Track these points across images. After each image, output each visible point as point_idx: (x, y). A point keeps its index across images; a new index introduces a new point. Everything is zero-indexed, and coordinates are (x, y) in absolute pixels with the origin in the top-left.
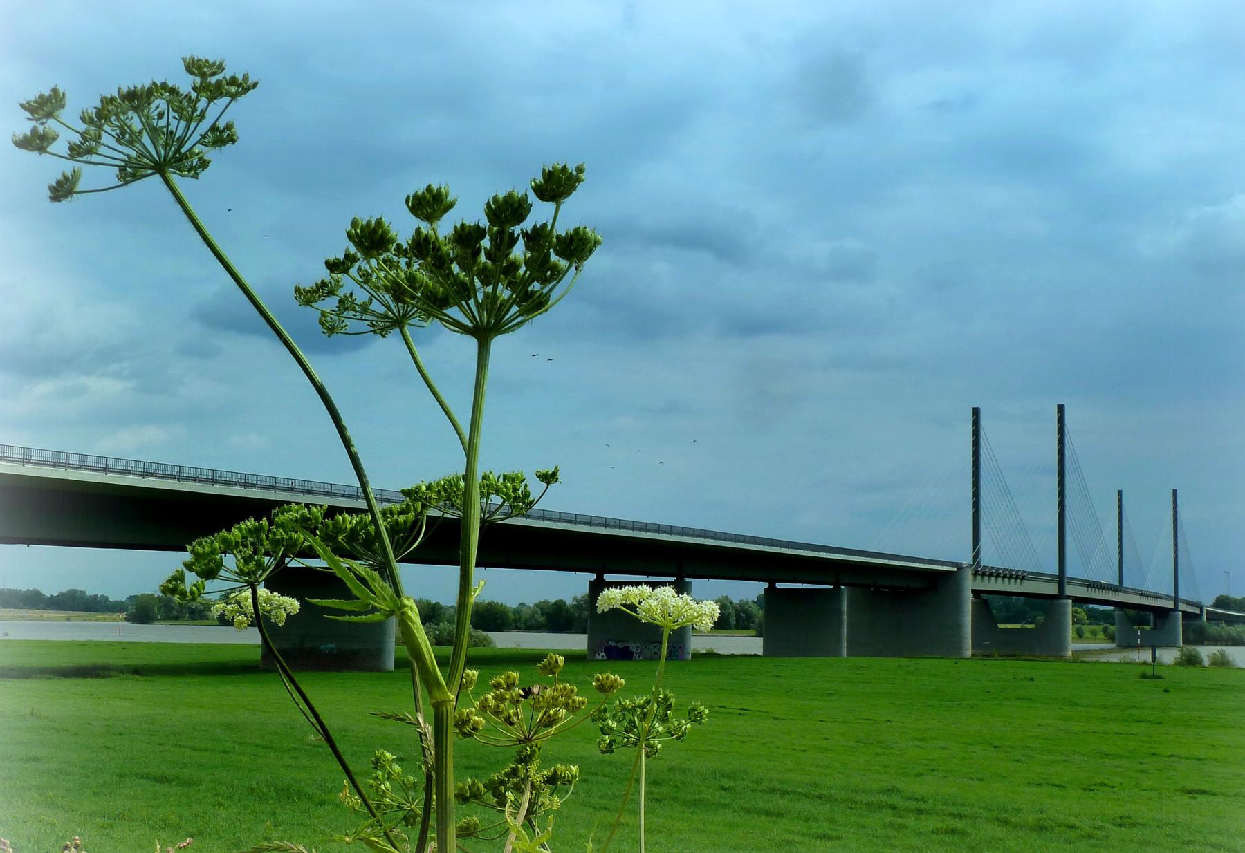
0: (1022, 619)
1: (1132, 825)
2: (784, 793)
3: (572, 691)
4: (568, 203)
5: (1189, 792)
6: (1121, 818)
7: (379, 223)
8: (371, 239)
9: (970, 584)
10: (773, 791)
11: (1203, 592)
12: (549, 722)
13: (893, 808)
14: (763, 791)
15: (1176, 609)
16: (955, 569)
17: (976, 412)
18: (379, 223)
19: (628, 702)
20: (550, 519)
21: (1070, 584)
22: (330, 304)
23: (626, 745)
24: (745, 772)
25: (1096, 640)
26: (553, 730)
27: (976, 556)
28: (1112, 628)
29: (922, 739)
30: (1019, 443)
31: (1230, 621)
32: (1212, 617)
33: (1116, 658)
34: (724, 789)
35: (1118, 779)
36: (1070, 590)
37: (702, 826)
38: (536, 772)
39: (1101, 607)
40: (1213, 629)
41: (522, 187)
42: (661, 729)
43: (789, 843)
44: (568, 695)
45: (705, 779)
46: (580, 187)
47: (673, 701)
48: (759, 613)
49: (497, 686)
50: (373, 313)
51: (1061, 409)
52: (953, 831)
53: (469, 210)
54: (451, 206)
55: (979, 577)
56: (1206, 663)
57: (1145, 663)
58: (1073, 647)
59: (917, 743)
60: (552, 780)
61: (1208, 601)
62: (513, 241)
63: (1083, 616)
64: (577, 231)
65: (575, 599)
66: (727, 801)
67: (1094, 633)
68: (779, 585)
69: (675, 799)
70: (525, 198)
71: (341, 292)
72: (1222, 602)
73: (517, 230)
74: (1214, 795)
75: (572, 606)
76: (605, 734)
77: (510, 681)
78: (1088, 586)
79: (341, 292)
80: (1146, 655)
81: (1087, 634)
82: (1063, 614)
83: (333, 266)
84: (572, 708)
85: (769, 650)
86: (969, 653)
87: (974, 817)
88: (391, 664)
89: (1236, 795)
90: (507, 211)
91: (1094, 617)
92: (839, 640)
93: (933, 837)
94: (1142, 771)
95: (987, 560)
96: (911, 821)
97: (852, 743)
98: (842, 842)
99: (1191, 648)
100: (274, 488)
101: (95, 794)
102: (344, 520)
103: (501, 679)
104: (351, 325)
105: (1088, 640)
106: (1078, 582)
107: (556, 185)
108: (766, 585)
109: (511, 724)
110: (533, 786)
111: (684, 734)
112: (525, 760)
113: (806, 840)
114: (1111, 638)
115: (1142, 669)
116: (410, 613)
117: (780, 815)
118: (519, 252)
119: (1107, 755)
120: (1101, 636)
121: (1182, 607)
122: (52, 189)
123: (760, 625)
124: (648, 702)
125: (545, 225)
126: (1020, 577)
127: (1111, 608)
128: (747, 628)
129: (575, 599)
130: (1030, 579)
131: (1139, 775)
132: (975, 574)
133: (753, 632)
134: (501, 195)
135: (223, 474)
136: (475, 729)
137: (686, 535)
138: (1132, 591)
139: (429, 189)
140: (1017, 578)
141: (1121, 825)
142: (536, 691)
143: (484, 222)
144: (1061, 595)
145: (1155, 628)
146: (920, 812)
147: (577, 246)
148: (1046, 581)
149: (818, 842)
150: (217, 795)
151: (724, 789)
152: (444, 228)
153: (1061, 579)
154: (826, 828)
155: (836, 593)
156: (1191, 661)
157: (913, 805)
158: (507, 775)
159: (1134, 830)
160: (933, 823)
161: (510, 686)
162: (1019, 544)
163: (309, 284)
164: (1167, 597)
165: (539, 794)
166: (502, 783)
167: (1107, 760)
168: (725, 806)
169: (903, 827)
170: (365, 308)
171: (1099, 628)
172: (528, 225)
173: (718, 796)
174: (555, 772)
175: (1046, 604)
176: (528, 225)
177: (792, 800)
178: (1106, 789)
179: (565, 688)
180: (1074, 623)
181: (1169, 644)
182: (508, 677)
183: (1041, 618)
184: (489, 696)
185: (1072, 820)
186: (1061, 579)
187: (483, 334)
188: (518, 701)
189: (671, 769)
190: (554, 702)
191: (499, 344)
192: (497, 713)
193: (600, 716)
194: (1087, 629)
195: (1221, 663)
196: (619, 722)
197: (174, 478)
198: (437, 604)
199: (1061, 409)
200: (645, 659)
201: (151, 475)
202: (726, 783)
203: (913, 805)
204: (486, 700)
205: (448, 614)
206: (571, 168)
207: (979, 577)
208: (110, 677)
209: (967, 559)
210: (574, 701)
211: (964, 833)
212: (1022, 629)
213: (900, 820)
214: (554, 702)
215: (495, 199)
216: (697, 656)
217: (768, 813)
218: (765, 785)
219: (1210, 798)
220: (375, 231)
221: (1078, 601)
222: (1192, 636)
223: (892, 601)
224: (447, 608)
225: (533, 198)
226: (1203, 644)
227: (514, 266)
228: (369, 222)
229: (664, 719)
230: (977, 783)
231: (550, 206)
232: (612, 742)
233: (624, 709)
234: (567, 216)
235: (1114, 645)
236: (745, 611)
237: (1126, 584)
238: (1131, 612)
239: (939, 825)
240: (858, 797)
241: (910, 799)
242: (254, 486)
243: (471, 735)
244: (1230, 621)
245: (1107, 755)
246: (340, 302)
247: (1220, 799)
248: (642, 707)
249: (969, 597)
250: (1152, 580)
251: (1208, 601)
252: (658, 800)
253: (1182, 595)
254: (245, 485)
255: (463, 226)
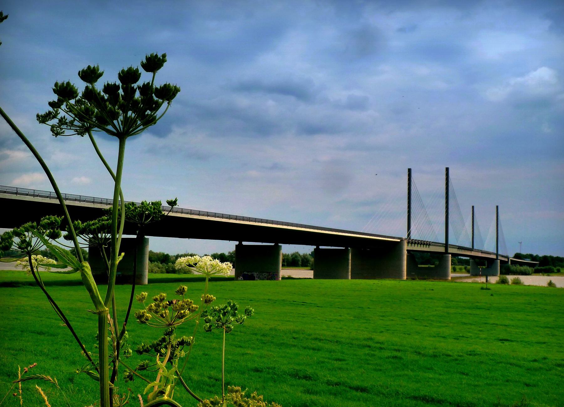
0: (429, 263)
1: (475, 355)
2: (320, 340)
3: (191, 302)
4: (159, 72)
5: (501, 340)
6: (470, 351)
7: (68, 84)
8: (64, 92)
9: (406, 247)
10: (316, 339)
11: (509, 251)
12: (182, 316)
13: (369, 347)
14: (312, 339)
15: (497, 259)
16: (399, 241)
17: (410, 170)
18: (68, 84)
19: (217, 307)
20: (218, 217)
21: (450, 247)
22: (55, 122)
23: (217, 327)
24: (304, 331)
25: (462, 273)
26: (183, 320)
27: (409, 235)
28: (469, 267)
29: (383, 316)
30: (429, 184)
31: (522, 264)
32: (513, 262)
33: (470, 280)
34: (295, 338)
35: (470, 334)
36: (450, 250)
37: (284, 355)
38: (174, 339)
39: (462, 257)
40: (513, 268)
41: (136, 65)
42: (233, 319)
43: (323, 362)
44: (189, 304)
45: (286, 334)
46: (165, 64)
47: (238, 306)
48: (312, 260)
49: (156, 300)
50: (76, 126)
51: (447, 169)
52: (395, 357)
53: (110, 77)
54: (101, 75)
55: (410, 244)
56: (510, 282)
57: (483, 283)
58: (451, 275)
59: (381, 318)
60: (182, 343)
61: (511, 255)
62: (134, 91)
63: (456, 261)
64: (165, 85)
65: (229, 253)
66: (295, 344)
67: (461, 269)
68: (321, 247)
69: (272, 342)
70: (137, 70)
71: (59, 117)
72: (518, 256)
73: (135, 85)
74: (512, 341)
75: (228, 256)
76: (207, 323)
77: (162, 298)
78: (458, 248)
79: (59, 117)
80: (483, 279)
81: (458, 270)
82: (447, 261)
83: (52, 104)
84: (192, 310)
85: (316, 276)
86: (405, 278)
87: (405, 351)
88: (146, 282)
89: (521, 341)
90: (128, 76)
91: (461, 262)
92: (348, 272)
93: (387, 360)
94: (481, 331)
95: (414, 237)
96: (377, 353)
97: (352, 318)
98: (346, 362)
99: (504, 276)
100: (93, 202)
101: (10, 340)
102: (78, 223)
103: (158, 297)
104: (67, 132)
105: (458, 272)
106: (454, 246)
107: (154, 64)
108: (315, 247)
109: (164, 317)
110: (172, 346)
111: (243, 321)
112: (169, 334)
113: (330, 361)
114: (468, 272)
115: (480, 286)
116: (86, 270)
117: (319, 350)
118: (137, 95)
119: (465, 324)
120: (464, 270)
121: (500, 258)
122: (148, 59)
123: (312, 265)
124: (226, 307)
125: (149, 83)
126: (428, 244)
127: (468, 258)
128: (306, 266)
129: (229, 253)
130: (433, 245)
131: (479, 332)
132: (408, 243)
133: (309, 268)
134: (126, 69)
135: (70, 196)
136: (147, 320)
137: (279, 224)
138: (478, 251)
139: (89, 67)
140: (427, 244)
141: (470, 355)
142: (174, 302)
143: (118, 83)
144: (447, 252)
145: (488, 267)
146: (381, 348)
147: (168, 93)
148: (440, 246)
149: (335, 362)
150: (66, 340)
151: (295, 338)
152: (99, 86)
153: (446, 245)
154: (339, 356)
155: (345, 252)
156: (504, 282)
157: (379, 345)
158: (160, 341)
159: (476, 357)
160: (387, 354)
161: (162, 300)
162: (428, 230)
163: (42, 113)
164: (493, 254)
165: (174, 350)
166: (158, 345)
167: (465, 326)
168: (294, 346)
169: (373, 355)
170: (72, 123)
171: (463, 267)
172: (140, 83)
173: (292, 342)
174: (183, 340)
175: (440, 257)
176: (140, 83)
177: (324, 343)
178: (464, 339)
179: (188, 301)
180: (452, 265)
181: (494, 275)
182: (161, 296)
183: (437, 263)
184: (153, 305)
185: (450, 353)
186: (446, 245)
187: (122, 136)
188: (166, 307)
189: (271, 329)
190: (182, 307)
191: (129, 143)
192: (156, 312)
193: (204, 315)
194: (457, 267)
195: (517, 282)
196: (213, 317)
197: (47, 197)
198: (167, 255)
199: (447, 169)
200: (261, 279)
201: (37, 196)
202: (295, 335)
203: (379, 345)
204: (151, 306)
205: (172, 259)
206: (160, 55)
207: (410, 244)
208: (19, 287)
209: (405, 236)
210: (192, 307)
211: (401, 358)
212: (429, 267)
213: (372, 352)
214: (182, 307)
215: (123, 71)
216: (283, 278)
217: (314, 349)
218: (313, 336)
219: (510, 343)
220: (66, 87)
221: (454, 255)
222: (504, 271)
223: (373, 256)
224: (172, 257)
225: (141, 70)
226: (509, 274)
227: (136, 102)
228: (63, 84)
229: (234, 315)
230: (407, 336)
231: (151, 74)
232: (210, 326)
233: (215, 310)
234: (160, 79)
235: (469, 275)
236: (306, 259)
237: (475, 247)
238: (477, 260)
239: (390, 355)
240: (354, 342)
241: (377, 343)
242: (84, 201)
243: (145, 323)
244: (522, 264)
245: (465, 324)
246: (60, 121)
247: (514, 343)
248: (223, 309)
249: (405, 253)
250: (487, 245)
251: (511, 255)
252: (264, 343)
253: (500, 253)
254: (80, 201)
255: (108, 84)
